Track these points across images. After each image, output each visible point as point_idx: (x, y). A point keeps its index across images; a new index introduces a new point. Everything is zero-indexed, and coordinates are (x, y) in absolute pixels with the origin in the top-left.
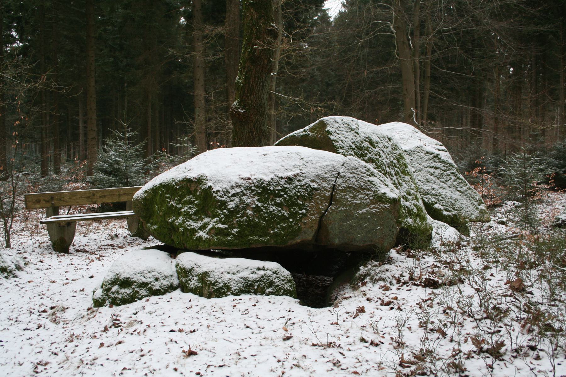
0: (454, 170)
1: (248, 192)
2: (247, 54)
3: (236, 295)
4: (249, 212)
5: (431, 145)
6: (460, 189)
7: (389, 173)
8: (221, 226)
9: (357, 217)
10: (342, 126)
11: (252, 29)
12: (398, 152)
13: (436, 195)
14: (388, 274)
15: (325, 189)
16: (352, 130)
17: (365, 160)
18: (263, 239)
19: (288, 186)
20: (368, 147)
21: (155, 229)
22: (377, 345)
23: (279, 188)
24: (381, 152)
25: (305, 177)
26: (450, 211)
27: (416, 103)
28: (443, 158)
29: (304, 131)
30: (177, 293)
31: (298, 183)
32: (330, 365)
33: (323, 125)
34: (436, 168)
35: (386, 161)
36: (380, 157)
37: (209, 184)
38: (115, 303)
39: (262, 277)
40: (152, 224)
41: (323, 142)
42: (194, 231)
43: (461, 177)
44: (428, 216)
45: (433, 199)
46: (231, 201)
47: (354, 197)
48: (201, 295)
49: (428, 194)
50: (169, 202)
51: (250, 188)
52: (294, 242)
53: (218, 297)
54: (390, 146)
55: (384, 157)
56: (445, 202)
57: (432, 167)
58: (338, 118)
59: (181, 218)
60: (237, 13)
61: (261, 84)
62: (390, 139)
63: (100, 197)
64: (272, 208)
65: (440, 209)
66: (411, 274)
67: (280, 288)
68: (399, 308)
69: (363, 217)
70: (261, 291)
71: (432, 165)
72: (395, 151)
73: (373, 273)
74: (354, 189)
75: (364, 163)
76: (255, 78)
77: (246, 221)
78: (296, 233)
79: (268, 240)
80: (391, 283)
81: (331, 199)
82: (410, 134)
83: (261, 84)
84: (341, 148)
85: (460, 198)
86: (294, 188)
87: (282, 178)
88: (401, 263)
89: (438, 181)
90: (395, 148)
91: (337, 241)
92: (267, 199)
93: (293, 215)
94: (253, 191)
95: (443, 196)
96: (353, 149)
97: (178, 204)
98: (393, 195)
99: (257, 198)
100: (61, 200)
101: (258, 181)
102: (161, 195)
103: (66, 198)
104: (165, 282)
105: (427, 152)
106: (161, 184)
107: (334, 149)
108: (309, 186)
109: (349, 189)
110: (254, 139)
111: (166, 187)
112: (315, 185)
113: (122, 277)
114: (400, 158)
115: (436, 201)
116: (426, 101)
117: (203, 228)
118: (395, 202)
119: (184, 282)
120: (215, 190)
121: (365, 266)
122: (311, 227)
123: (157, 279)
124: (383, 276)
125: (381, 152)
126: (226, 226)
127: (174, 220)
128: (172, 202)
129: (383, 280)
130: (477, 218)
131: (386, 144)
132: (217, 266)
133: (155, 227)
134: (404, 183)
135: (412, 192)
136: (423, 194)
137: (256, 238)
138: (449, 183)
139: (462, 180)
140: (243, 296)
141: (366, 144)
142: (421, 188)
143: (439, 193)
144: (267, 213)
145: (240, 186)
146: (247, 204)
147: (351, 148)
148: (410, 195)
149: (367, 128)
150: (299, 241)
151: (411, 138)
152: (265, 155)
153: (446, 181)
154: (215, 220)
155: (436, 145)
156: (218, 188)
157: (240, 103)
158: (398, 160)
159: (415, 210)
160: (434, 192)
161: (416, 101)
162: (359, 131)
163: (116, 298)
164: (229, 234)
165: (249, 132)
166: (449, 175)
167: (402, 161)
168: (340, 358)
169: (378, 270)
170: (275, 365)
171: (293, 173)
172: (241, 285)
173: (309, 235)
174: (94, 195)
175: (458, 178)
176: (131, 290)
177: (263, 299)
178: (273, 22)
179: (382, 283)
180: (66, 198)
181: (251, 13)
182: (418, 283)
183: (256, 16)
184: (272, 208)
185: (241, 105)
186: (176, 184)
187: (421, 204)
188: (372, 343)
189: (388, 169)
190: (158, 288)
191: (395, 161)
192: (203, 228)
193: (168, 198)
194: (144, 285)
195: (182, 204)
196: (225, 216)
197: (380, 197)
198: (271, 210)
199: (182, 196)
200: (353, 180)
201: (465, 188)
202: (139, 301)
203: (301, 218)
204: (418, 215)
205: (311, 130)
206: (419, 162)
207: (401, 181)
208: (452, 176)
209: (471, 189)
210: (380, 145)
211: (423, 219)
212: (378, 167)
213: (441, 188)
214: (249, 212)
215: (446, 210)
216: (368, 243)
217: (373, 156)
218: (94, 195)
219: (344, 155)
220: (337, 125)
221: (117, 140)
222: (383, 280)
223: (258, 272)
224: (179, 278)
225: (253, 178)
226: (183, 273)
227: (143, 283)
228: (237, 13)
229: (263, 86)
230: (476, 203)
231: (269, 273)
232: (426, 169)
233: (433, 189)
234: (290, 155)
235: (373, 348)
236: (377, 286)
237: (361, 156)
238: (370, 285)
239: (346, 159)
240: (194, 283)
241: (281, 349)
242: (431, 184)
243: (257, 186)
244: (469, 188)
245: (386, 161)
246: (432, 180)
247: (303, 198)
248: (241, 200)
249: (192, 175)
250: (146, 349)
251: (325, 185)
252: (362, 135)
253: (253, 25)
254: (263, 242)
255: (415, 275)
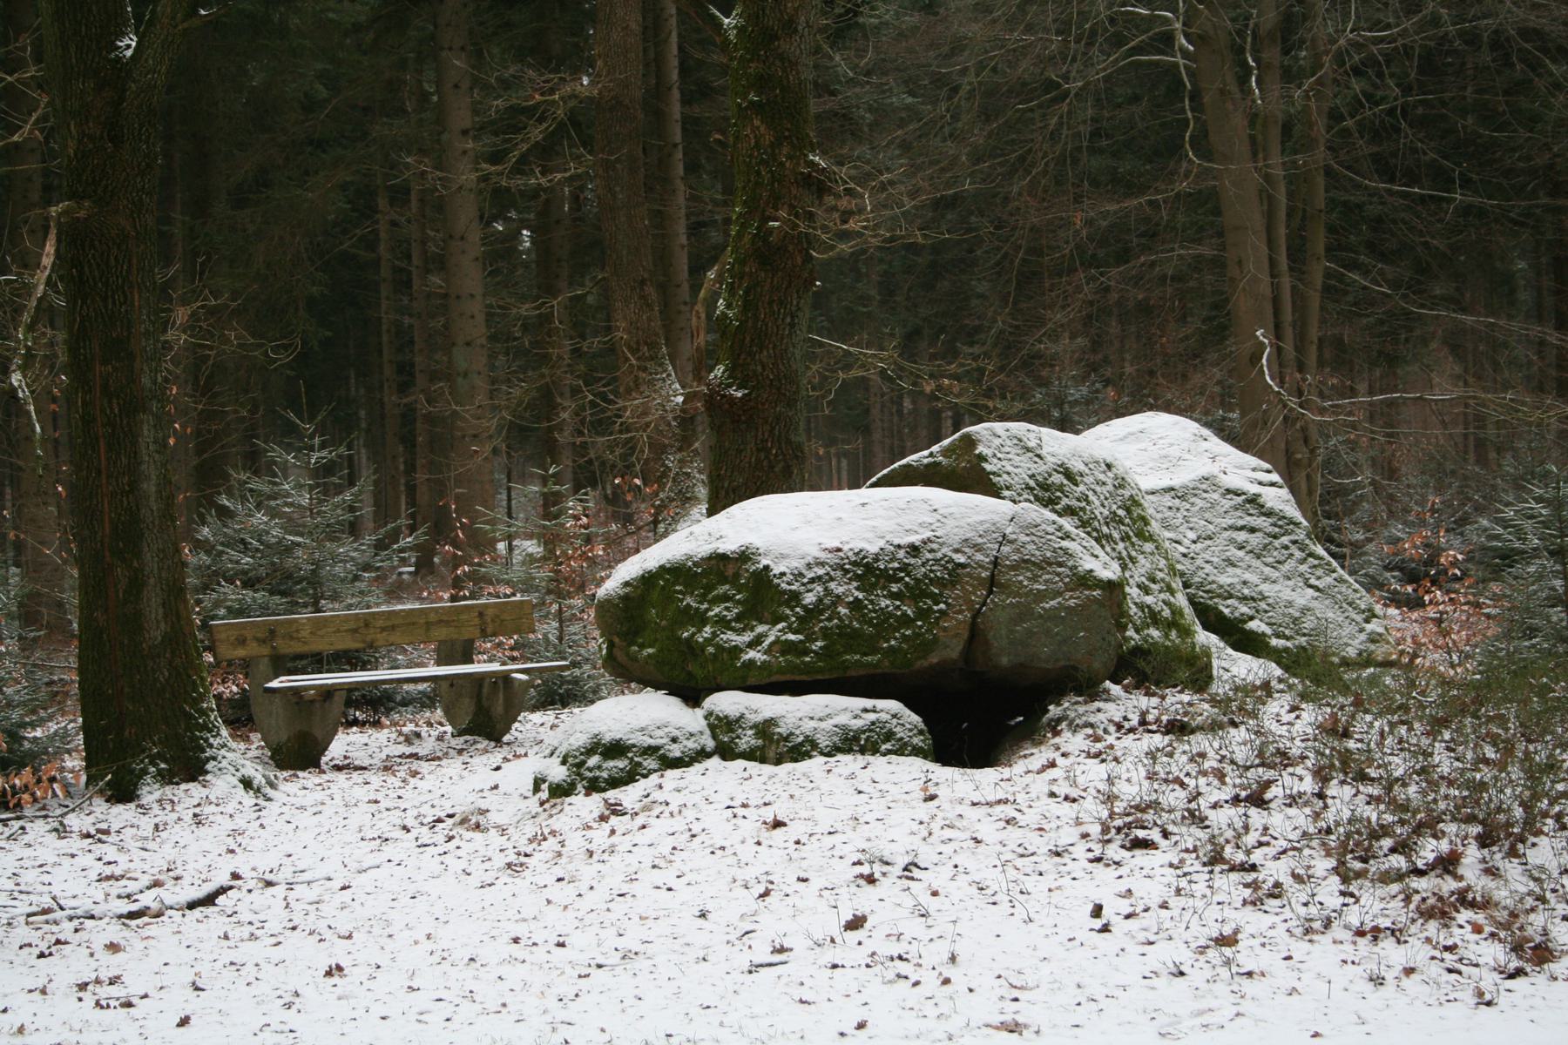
0: (1301, 535)
1: (839, 573)
2: (747, 238)
3: (829, 755)
4: (843, 611)
5: (1241, 469)
6: (1316, 583)
7: (1109, 537)
8: (792, 637)
9: (1041, 616)
10: (1008, 442)
11: (758, 173)
12: (1127, 493)
13: (1253, 599)
14: (1101, 716)
15: (980, 565)
16: (1028, 450)
17: (1056, 512)
18: (869, 658)
19: (912, 561)
20: (1062, 485)
21: (649, 655)
22: (1074, 800)
23: (896, 565)
24: (1090, 494)
25: (941, 544)
26: (1288, 638)
27: (1277, 312)
28: (1269, 505)
29: (931, 455)
30: (715, 762)
31: (929, 556)
32: (1003, 824)
33: (970, 442)
34: (1253, 530)
35: (1101, 512)
36: (1088, 503)
37: (765, 562)
38: (593, 787)
39: (873, 723)
40: (642, 646)
41: (969, 475)
42: (736, 651)
43: (1320, 550)
44: (1198, 628)
45: (1244, 609)
46: (809, 591)
47: (1034, 579)
48: (763, 761)
49: (1231, 596)
50: (681, 601)
51: (841, 567)
52: (925, 663)
53: (796, 761)
54: (1109, 481)
55: (1097, 503)
56: (1276, 616)
57: (1242, 528)
58: (999, 427)
59: (708, 629)
60: (634, 26)
61: (788, 320)
62: (1109, 466)
63: (383, 629)
64: (884, 603)
65: (1264, 634)
66: (1143, 714)
67: (906, 744)
68: (1116, 759)
69: (1052, 615)
70: (870, 748)
71: (1240, 523)
72: (1120, 491)
73: (1072, 714)
74: (1034, 564)
75: (1054, 517)
76: (771, 302)
77: (838, 627)
78: (927, 647)
79: (879, 661)
80: (1106, 731)
81: (992, 583)
82: (1185, 445)
83: (788, 320)
84: (1008, 488)
85: (1315, 604)
86: (923, 564)
87: (899, 546)
88: (1123, 703)
89: (1256, 563)
90: (1121, 483)
91: (1005, 661)
92: (874, 586)
93: (923, 614)
94: (847, 571)
95: (1270, 601)
96: (1032, 489)
97: (701, 603)
98: (1108, 571)
99: (855, 584)
100: (292, 638)
101: (857, 554)
102: (663, 588)
103: (303, 634)
104: (691, 744)
105: (1228, 491)
106: (662, 567)
107: (994, 491)
108: (951, 560)
109: (1024, 564)
110: (772, 467)
111: (675, 573)
112: (961, 559)
113: (607, 738)
114: (1132, 504)
115: (1251, 612)
116: (1315, 300)
117: (752, 645)
118: (1114, 589)
119: (725, 742)
120: (776, 571)
121: (1058, 704)
122: (957, 635)
123: (674, 740)
124: (1092, 719)
125: (1090, 494)
126: (801, 637)
127: (694, 634)
128: (689, 600)
129: (1092, 726)
130: (1360, 654)
131: (1102, 477)
132: (789, 708)
133: (650, 651)
134: (1141, 557)
135: (1160, 575)
136: (1219, 596)
137: (857, 657)
138: (1286, 567)
139: (1322, 558)
140: (840, 757)
141: (1057, 479)
142: (1213, 582)
143: (1260, 593)
144: (875, 611)
145: (822, 564)
146: (838, 596)
147: (1028, 487)
148: (1154, 581)
149: (1057, 444)
150: (935, 660)
151: (1187, 456)
152: (863, 505)
153: (1279, 562)
154: (780, 626)
155: (1254, 470)
156: (783, 569)
157: (731, 371)
158: (1128, 511)
159: (1167, 613)
160: (1246, 591)
161: (1276, 302)
162: (1043, 452)
163: (596, 779)
164: (806, 652)
165: (758, 450)
166: (1286, 547)
167: (1136, 512)
168: (1017, 815)
169: (1081, 709)
170: (915, 827)
171: (920, 537)
172: (836, 739)
173: (953, 650)
174: (367, 625)
175: (1311, 555)
176: (626, 762)
177: (878, 762)
178: (813, 151)
179: (1089, 731)
180: (303, 634)
181: (755, 129)
182: (1154, 727)
183: (768, 138)
184: (884, 603)
185: (735, 379)
186: (696, 564)
187: (1181, 600)
188: (1066, 798)
189: (1105, 530)
190: (678, 754)
191: (1121, 512)
192: (752, 645)
193: (680, 592)
194: (651, 751)
195: (709, 602)
196: (799, 618)
197: (1083, 577)
198: (883, 605)
199: (709, 588)
200: (1031, 547)
201: (1329, 580)
202: (643, 781)
203: (937, 619)
204: (1174, 622)
205: (946, 452)
206: (1207, 515)
207: (1133, 553)
208: (1294, 549)
209: (1345, 581)
210: (1089, 480)
211: (1186, 632)
212: (1084, 524)
213: (1266, 580)
214: (843, 611)
215: (1278, 636)
216: (1062, 663)
217: (1074, 503)
218: (367, 625)
219: (1014, 502)
220: (997, 442)
221: (275, 475)
222: (1092, 726)
223: (865, 715)
224: (714, 737)
225: (846, 548)
226: (722, 726)
227: (650, 747)
228: (634, 26)
229: (792, 325)
230: (1359, 618)
231: (884, 716)
232: (1226, 534)
233: (1245, 583)
234: (913, 505)
235: (1066, 804)
236: (1080, 736)
237: (1048, 503)
238: (1067, 734)
239: (1017, 508)
240: (747, 740)
241: (924, 810)
242: (1238, 571)
243: (854, 563)
244: (1340, 580)
245: (1101, 512)
246: (1242, 560)
247: (938, 582)
248: (826, 589)
249: (729, 546)
250: (696, 828)
251: (979, 557)
252: (1050, 459)
253: (763, 162)
254: (869, 665)
255: (1150, 718)
